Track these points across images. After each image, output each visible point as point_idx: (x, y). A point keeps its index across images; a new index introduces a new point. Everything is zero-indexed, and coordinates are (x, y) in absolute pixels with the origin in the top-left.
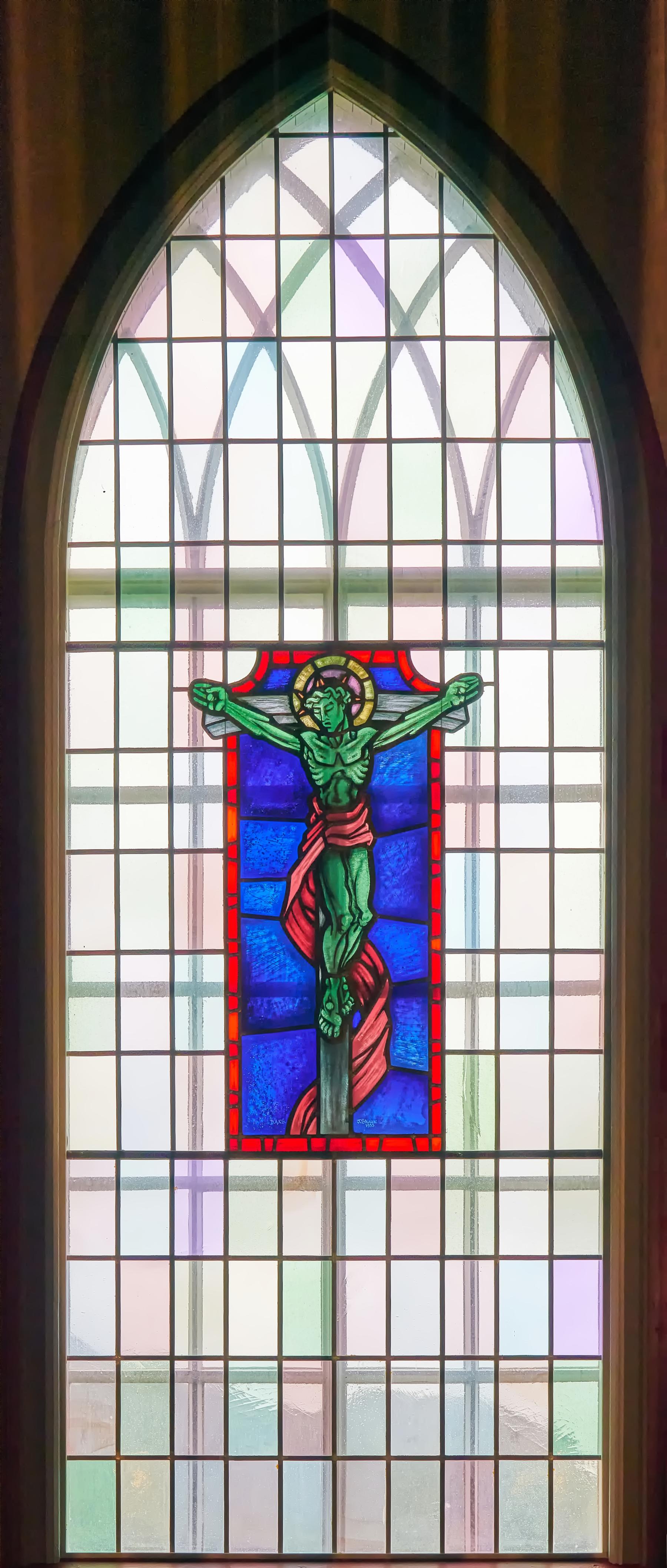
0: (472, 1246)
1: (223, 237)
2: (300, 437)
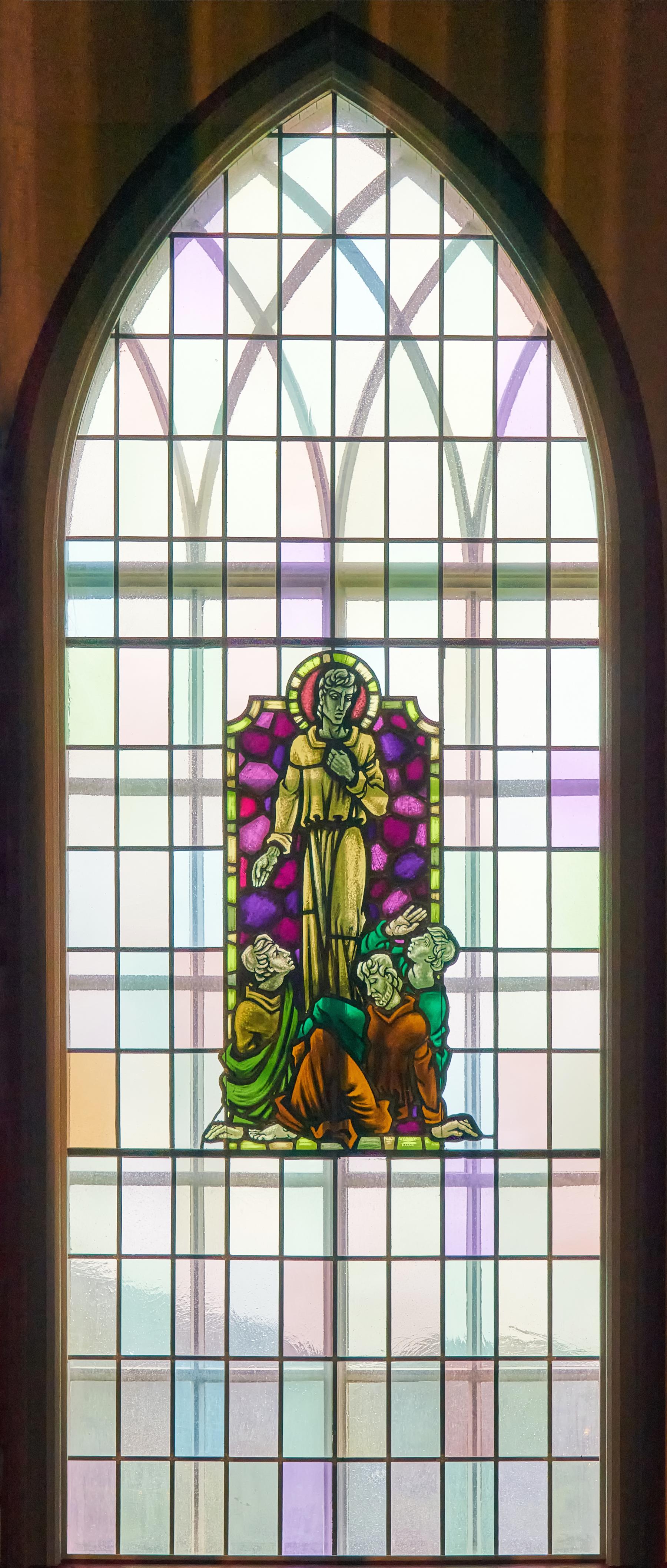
1: (226, 235)
2: (300, 434)
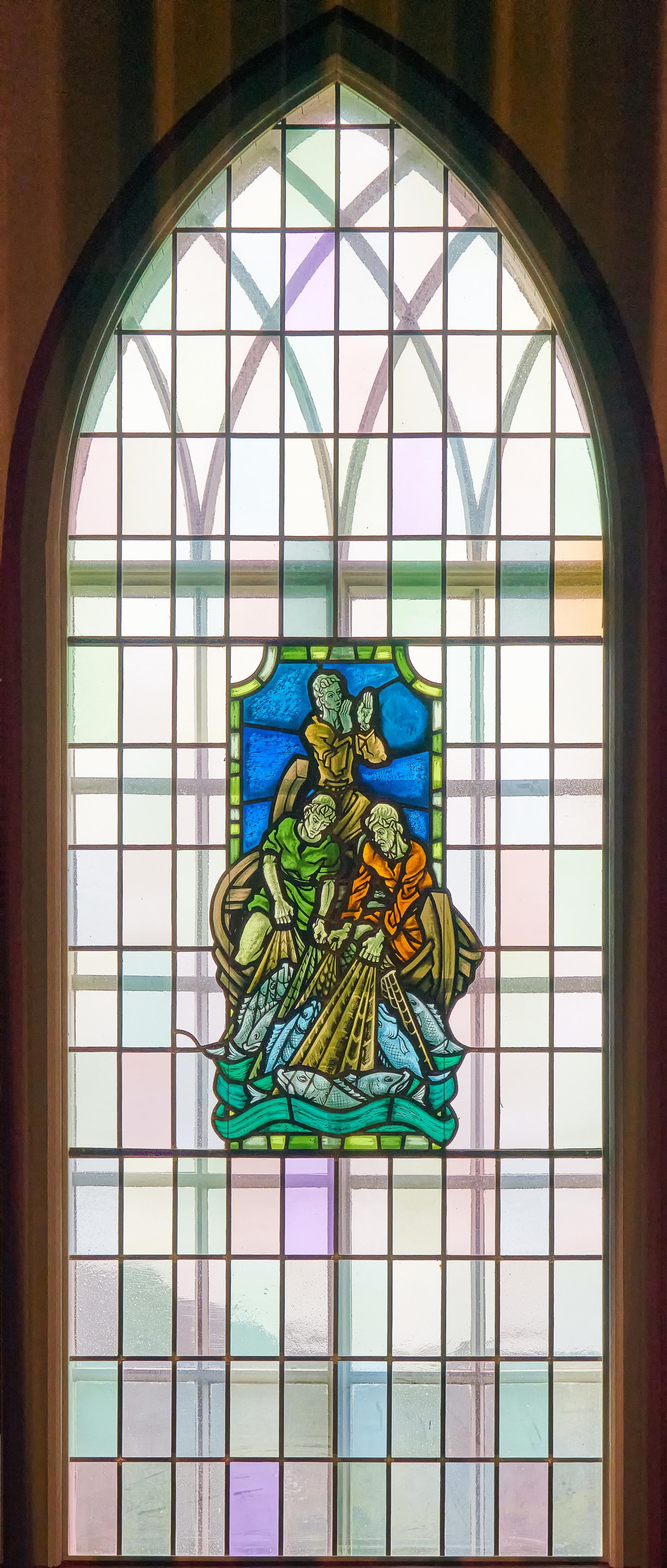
1: (229, 230)
2: (306, 431)
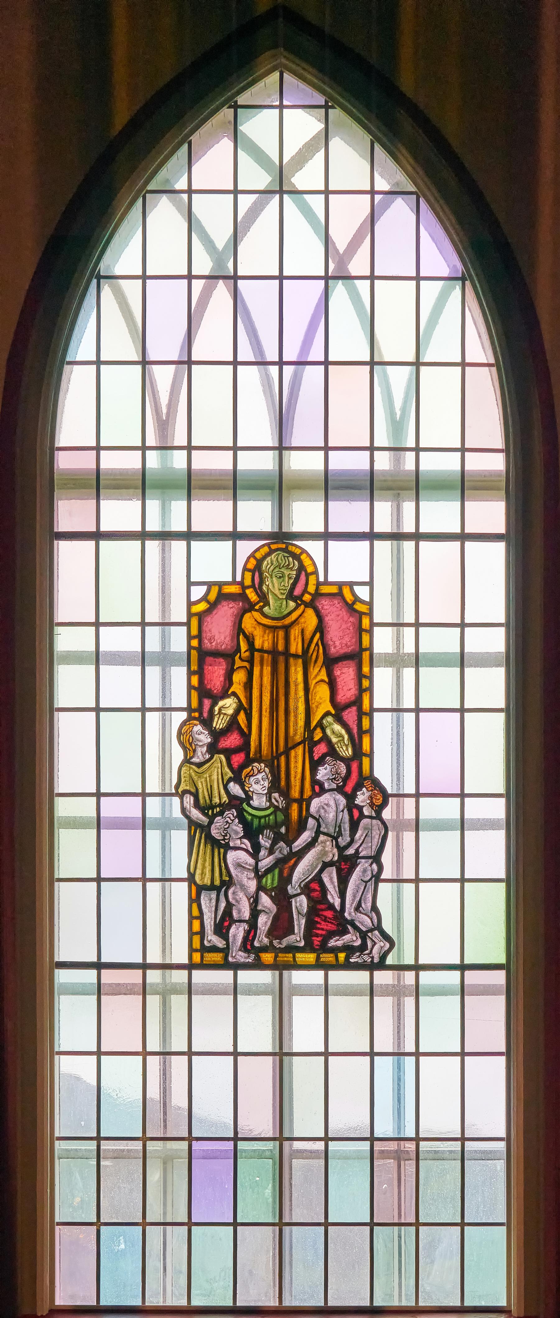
0: (399, 1046)
1: (190, 191)
